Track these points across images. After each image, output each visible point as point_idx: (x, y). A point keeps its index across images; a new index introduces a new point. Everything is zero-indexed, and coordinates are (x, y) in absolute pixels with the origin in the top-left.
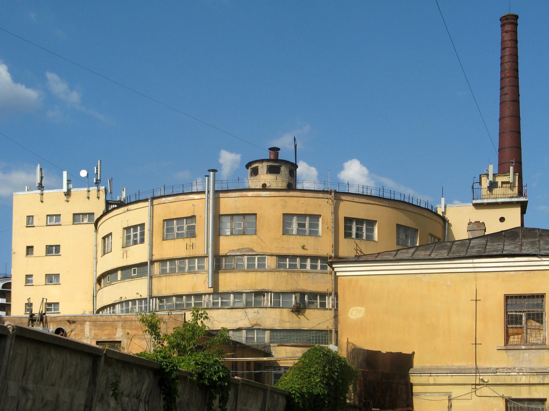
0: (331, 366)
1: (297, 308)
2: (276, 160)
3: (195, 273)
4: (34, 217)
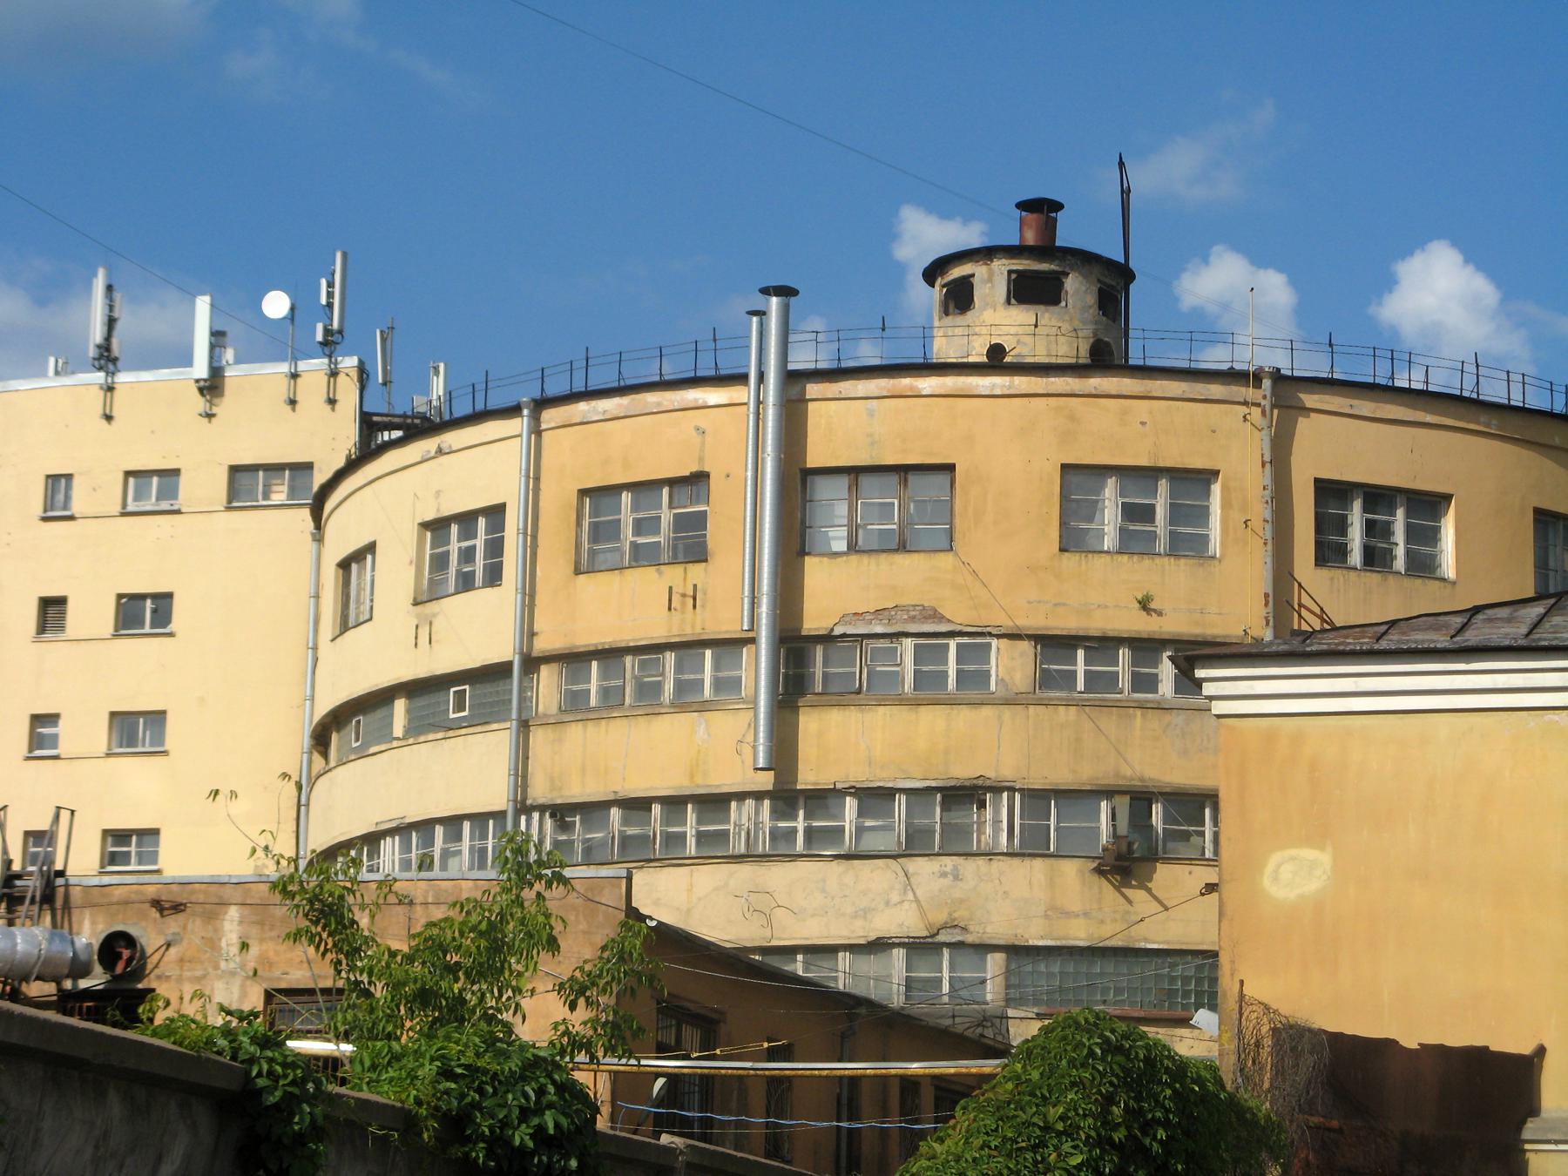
0: (1138, 1099)
1: (1119, 857)
2: (1046, 250)
3: (704, 707)
4: (76, 482)
